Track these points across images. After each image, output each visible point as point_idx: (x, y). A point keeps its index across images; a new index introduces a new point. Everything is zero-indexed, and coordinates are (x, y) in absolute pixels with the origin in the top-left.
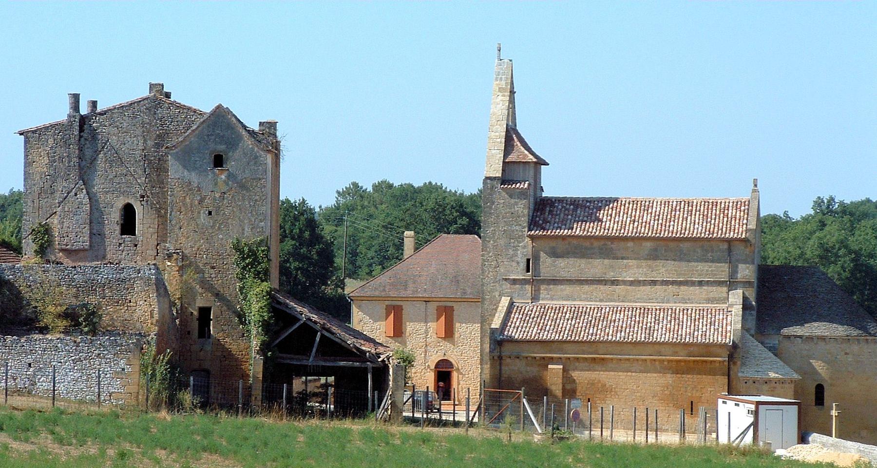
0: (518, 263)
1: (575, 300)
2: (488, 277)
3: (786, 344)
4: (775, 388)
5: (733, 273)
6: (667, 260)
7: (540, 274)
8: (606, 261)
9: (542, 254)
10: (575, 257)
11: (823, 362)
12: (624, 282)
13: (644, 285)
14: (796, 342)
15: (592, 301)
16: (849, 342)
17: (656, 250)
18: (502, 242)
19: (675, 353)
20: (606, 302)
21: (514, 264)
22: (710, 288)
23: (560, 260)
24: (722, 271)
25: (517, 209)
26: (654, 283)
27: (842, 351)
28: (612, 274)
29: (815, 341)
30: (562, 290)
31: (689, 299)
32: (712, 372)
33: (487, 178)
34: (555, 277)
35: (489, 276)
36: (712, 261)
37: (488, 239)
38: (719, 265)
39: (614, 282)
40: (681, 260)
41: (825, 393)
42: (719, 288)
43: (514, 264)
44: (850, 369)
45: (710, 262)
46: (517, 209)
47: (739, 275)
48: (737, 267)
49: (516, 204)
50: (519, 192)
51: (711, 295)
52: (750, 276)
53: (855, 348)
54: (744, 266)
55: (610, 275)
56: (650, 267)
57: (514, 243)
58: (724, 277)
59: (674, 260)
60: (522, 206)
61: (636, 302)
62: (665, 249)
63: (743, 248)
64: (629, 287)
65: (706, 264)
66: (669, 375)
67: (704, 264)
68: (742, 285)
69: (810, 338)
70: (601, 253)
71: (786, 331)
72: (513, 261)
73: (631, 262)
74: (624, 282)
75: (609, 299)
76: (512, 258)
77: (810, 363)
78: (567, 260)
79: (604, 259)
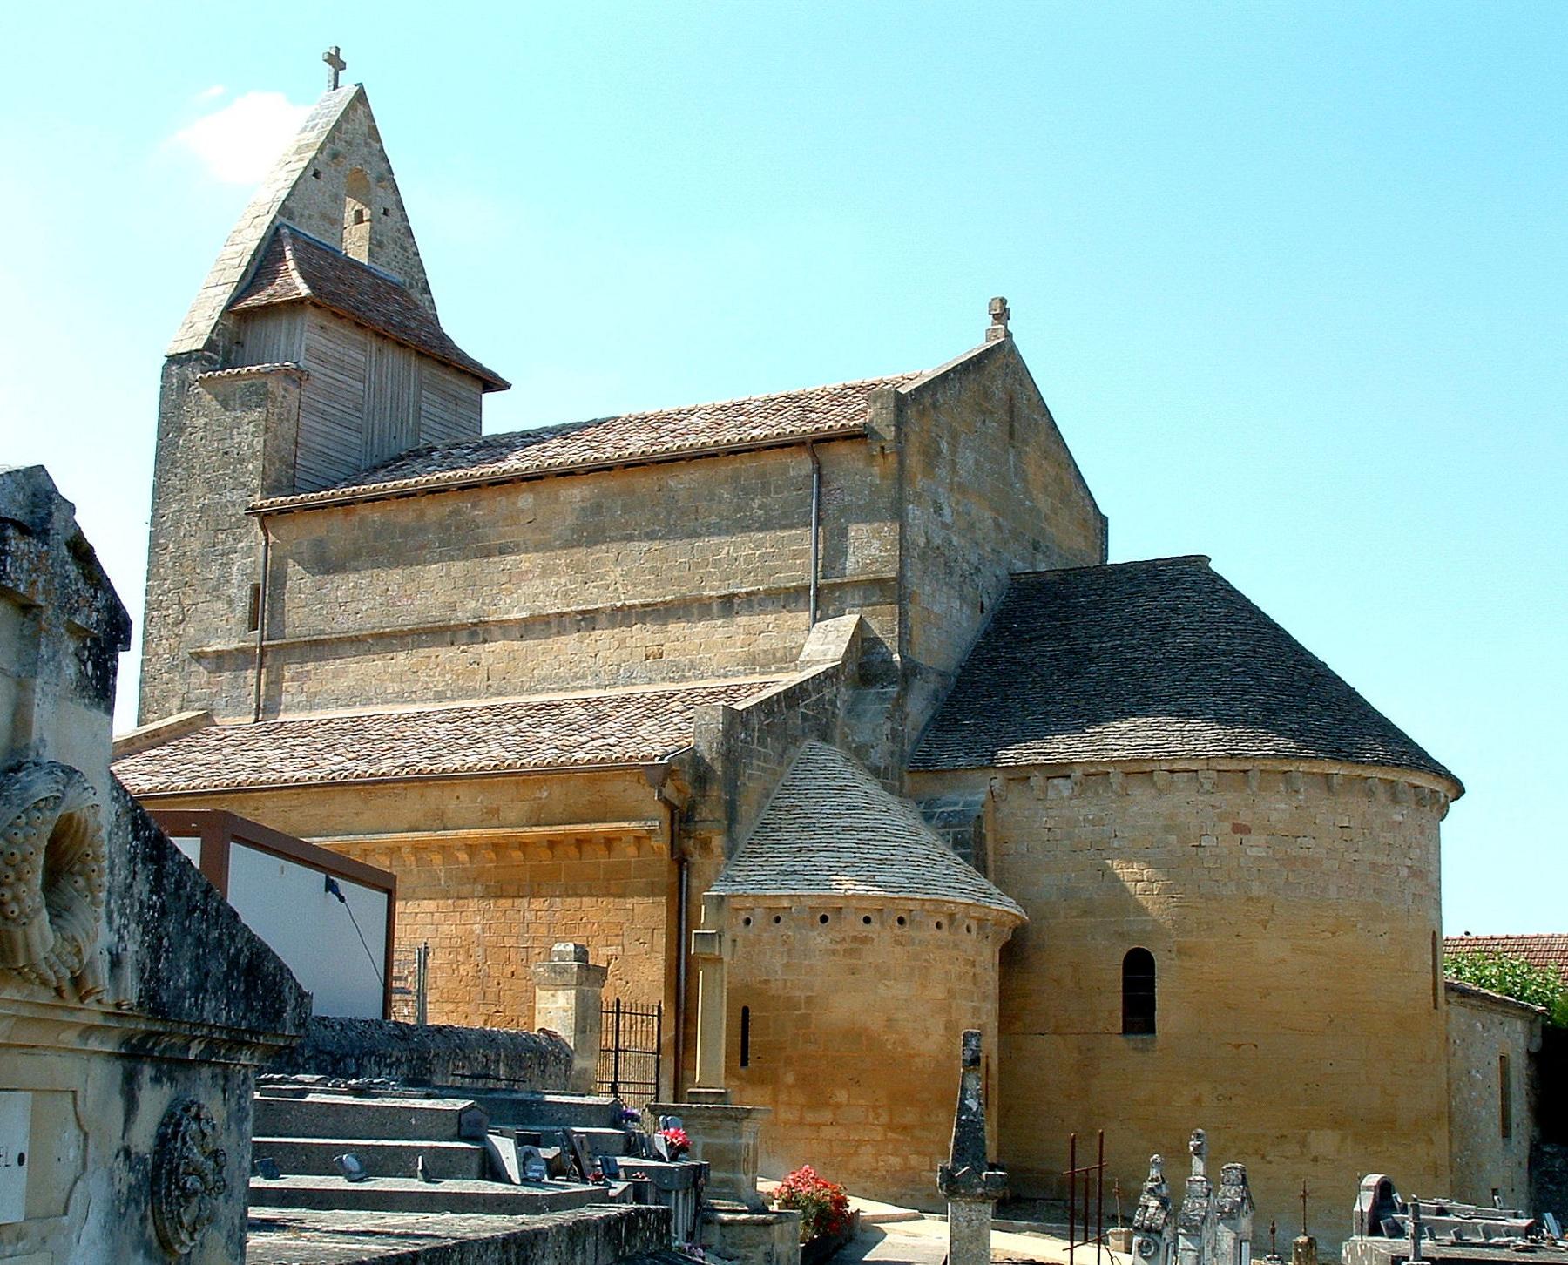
0: (230, 602)
1: (368, 702)
2: (157, 654)
3: (1017, 803)
4: (865, 940)
5: (833, 553)
6: (630, 538)
7: (283, 631)
8: (457, 567)
9: (294, 570)
10: (377, 565)
11: (1150, 865)
12: (505, 629)
13: (559, 634)
14: (1051, 794)
15: (413, 701)
16: (1247, 783)
17: (597, 509)
18: (195, 545)
19: (491, 816)
20: (453, 699)
21: (221, 606)
22: (759, 621)
23: (338, 579)
24: (796, 554)
25: (237, 439)
26: (588, 619)
27: (1222, 818)
28: (473, 604)
29: (1116, 779)
30: (337, 675)
31: (692, 665)
32: (613, 885)
33: (173, 359)
34: (322, 632)
35: (161, 652)
36: (765, 526)
37: (162, 541)
38: (786, 533)
39: (477, 631)
40: (671, 533)
41: (1159, 986)
42: (786, 616)
43: (221, 606)
44: (1256, 889)
45: (760, 530)
46: (237, 439)
47: (850, 564)
48: (844, 534)
49: (237, 423)
50: (247, 387)
51: (762, 644)
52: (885, 563)
53: (1278, 807)
54: (865, 527)
55: (467, 610)
56: (578, 568)
57: (224, 542)
58: (801, 572)
59: (651, 536)
60: (251, 428)
61: (537, 692)
62: (624, 505)
63: (861, 465)
64: (517, 645)
65: (745, 537)
66: (473, 905)
67: (738, 539)
68: (858, 597)
69: (1096, 774)
70: (443, 543)
71: (1010, 755)
72: (219, 598)
73: (526, 561)
74: (505, 629)
75: (461, 689)
76: (216, 588)
77: (1105, 872)
78: (353, 577)
79: (452, 559)
